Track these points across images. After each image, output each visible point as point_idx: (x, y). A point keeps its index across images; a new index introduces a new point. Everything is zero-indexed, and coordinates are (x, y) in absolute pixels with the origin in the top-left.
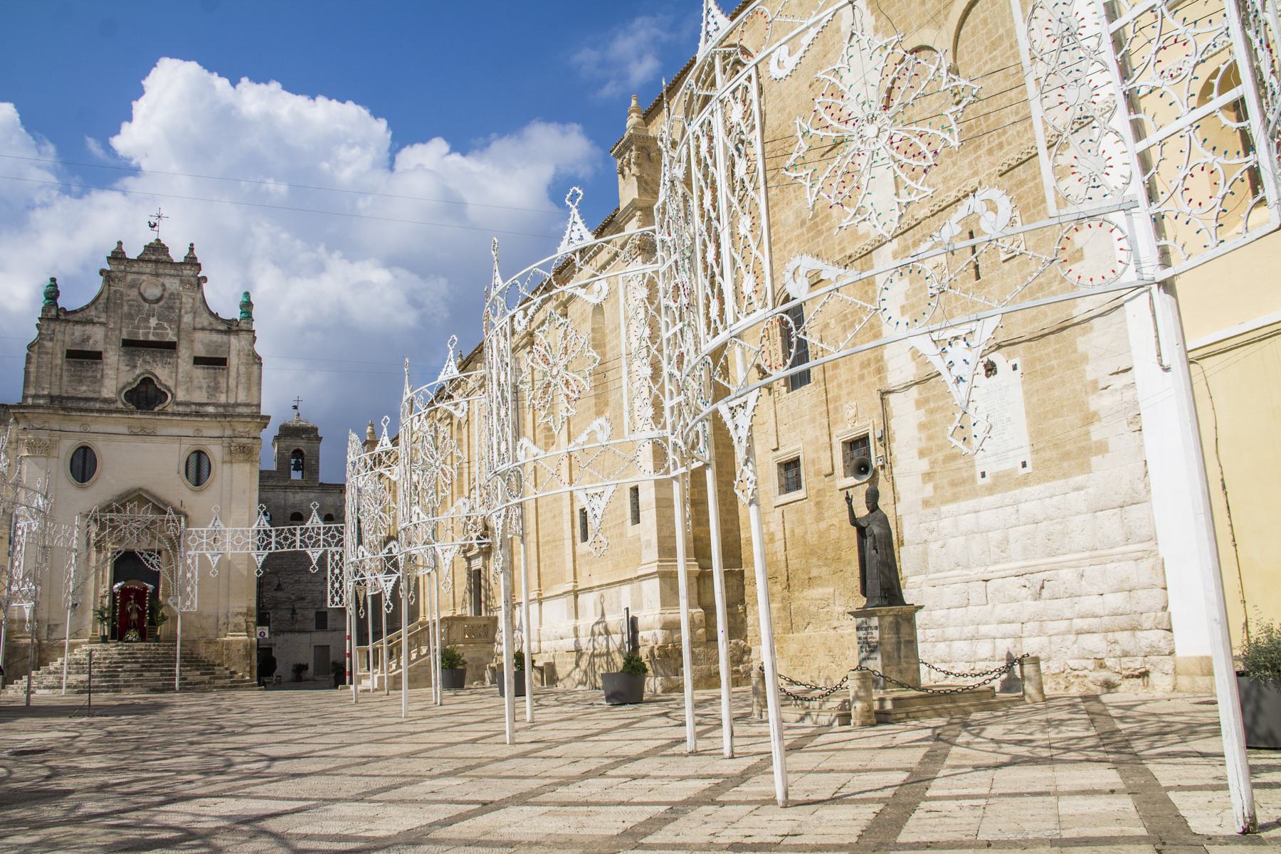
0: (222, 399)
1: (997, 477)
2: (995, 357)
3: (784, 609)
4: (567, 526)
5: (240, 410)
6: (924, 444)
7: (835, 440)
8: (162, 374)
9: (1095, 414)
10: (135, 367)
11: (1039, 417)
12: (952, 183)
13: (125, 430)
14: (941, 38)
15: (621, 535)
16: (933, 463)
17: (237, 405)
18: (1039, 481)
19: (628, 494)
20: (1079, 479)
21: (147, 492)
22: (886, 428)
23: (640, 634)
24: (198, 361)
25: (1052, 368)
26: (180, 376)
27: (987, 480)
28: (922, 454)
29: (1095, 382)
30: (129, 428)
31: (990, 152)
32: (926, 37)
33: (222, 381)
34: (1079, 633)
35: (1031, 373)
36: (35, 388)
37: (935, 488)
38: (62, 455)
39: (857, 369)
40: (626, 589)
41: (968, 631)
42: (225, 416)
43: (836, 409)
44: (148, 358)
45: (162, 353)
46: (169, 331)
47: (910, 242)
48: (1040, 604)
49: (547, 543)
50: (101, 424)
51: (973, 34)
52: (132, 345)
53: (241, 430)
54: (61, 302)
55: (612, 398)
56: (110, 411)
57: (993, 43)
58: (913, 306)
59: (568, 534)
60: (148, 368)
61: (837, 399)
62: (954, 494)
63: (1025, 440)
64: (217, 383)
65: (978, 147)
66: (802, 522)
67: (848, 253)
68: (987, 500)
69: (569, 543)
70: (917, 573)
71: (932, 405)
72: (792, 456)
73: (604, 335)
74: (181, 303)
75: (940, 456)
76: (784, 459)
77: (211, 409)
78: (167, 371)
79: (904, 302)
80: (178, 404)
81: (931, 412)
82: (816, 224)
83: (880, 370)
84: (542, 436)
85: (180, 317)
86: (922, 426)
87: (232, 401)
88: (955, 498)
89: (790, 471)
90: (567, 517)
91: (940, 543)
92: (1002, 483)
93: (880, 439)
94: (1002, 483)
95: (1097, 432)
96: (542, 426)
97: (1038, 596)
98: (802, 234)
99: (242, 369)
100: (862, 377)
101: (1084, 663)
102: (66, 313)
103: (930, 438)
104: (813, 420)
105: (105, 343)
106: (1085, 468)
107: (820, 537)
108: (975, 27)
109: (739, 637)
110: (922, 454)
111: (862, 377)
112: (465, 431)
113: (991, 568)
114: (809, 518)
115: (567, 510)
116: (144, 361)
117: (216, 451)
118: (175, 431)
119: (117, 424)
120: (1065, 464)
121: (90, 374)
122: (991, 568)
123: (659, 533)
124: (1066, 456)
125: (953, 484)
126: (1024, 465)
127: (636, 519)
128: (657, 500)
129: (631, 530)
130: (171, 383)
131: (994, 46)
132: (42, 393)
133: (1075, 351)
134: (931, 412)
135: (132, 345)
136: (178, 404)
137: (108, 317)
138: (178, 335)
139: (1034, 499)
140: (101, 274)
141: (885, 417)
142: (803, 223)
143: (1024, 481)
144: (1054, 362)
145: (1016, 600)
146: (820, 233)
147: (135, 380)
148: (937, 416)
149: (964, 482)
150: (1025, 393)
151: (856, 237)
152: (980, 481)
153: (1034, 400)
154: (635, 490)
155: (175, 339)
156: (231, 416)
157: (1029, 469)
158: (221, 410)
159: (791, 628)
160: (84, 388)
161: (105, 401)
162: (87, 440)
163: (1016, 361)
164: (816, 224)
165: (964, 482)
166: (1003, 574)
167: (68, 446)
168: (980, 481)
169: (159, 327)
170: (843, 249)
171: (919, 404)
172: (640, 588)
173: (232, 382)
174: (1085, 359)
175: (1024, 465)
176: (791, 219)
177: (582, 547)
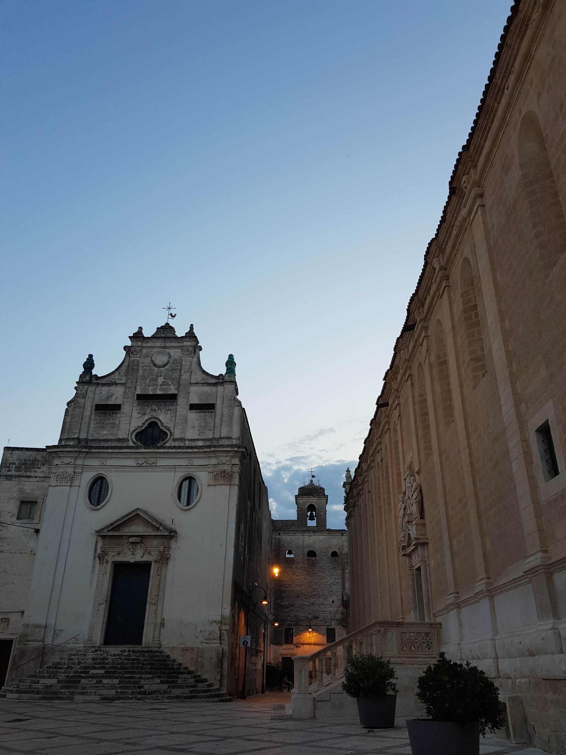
0: (210, 435)
10: (144, 414)
17: (220, 438)
33: (210, 421)
44: (154, 407)
60: (154, 414)
77: (200, 443)
87: (217, 436)
121: (111, 421)
130: (170, 425)
138: (178, 389)
155: (176, 392)
160: (105, 432)
169: (164, 384)
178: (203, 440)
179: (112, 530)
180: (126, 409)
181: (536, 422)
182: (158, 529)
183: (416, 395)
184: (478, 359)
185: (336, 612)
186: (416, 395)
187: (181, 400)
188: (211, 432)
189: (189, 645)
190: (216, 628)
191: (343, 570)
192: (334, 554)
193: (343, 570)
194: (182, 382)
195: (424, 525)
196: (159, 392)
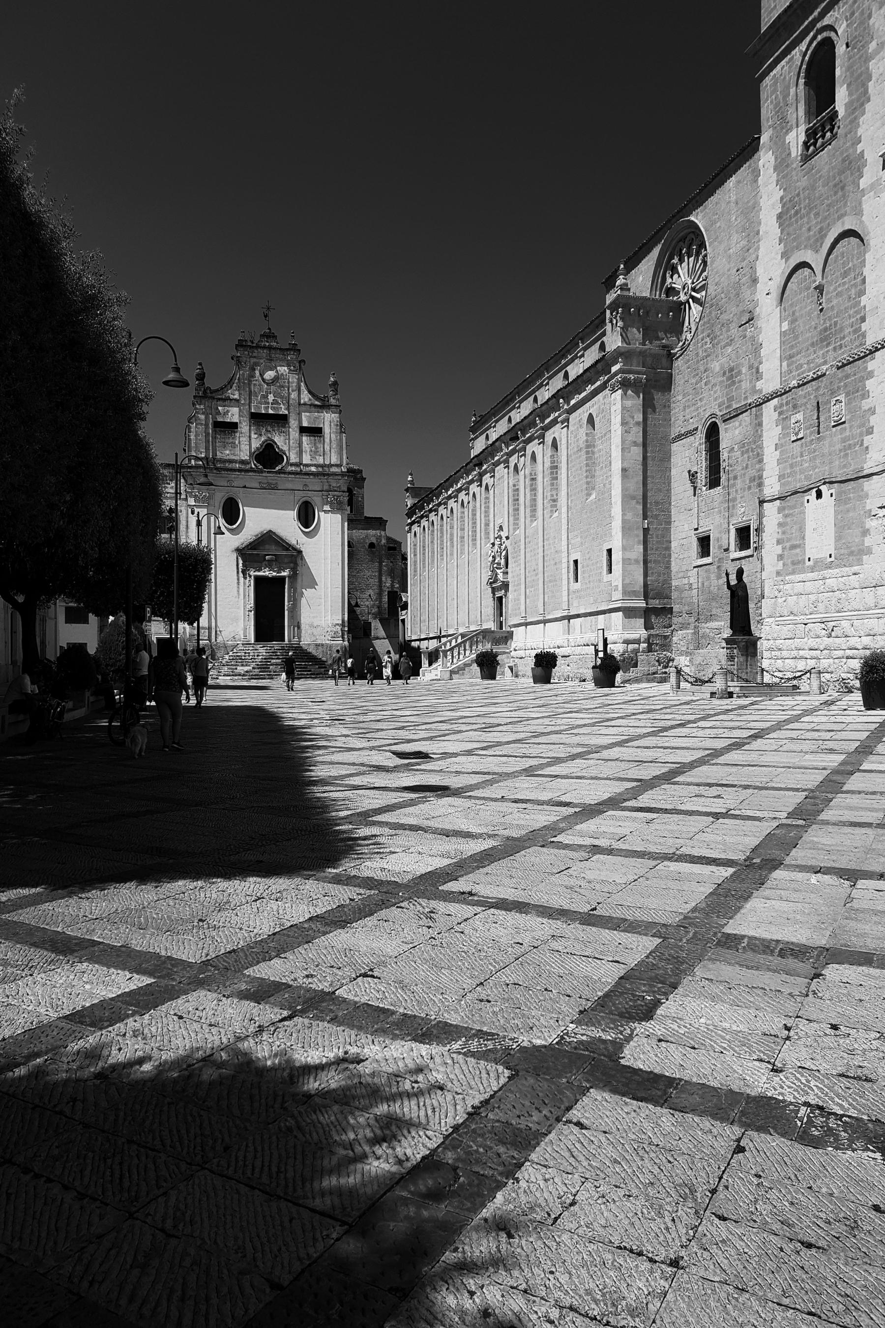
0: (321, 460)
1: (816, 562)
2: (824, 488)
3: (694, 633)
4: (565, 571)
5: (334, 469)
6: (780, 536)
7: (731, 527)
8: (279, 440)
9: (868, 530)
10: (261, 435)
11: (841, 528)
12: (812, 365)
13: (257, 485)
14: (816, 260)
15: (600, 581)
16: (784, 549)
17: (331, 465)
18: (838, 566)
19: (605, 553)
20: (856, 569)
21: (274, 533)
22: (761, 523)
23: (609, 646)
24: (303, 430)
25: (850, 499)
26: (291, 442)
27: (811, 563)
28: (779, 542)
29: (870, 511)
30: (260, 483)
31: (835, 349)
32: (808, 256)
33: (320, 446)
34: (848, 658)
35: (840, 500)
36: (195, 451)
37: (784, 565)
38: (217, 504)
39: (748, 482)
40: (601, 617)
41: (794, 653)
42: (324, 475)
43: (733, 506)
44: (269, 428)
45: (278, 423)
46: (282, 406)
47: (784, 402)
48: (831, 639)
49: (550, 581)
50: (239, 480)
51: (835, 262)
52: (258, 419)
53: (334, 485)
54: (208, 383)
55: (599, 481)
56: (247, 471)
57: (845, 272)
58: (782, 445)
59: (565, 577)
60: (270, 436)
61: (735, 499)
62: (793, 570)
63: (832, 541)
64: (316, 448)
65: (828, 344)
66: (708, 578)
67: (749, 401)
68: (811, 575)
69: (565, 582)
70: (770, 617)
71: (787, 512)
72: (706, 534)
73: (594, 440)
74: (289, 382)
75: (788, 545)
76: (701, 535)
77: (313, 469)
78: (282, 438)
79: (777, 442)
80: (292, 465)
81: (786, 516)
82: (732, 376)
83: (760, 485)
84: (549, 505)
85: (289, 394)
86: (780, 525)
87: (327, 462)
88: (793, 573)
89: (704, 543)
90: (565, 565)
91: (784, 599)
92: (819, 565)
93: (756, 530)
94: (819, 565)
95: (868, 541)
96: (549, 498)
97: (830, 636)
98: (723, 381)
99: (333, 436)
100: (749, 488)
101: (849, 675)
102: (212, 392)
103: (784, 533)
104: (720, 512)
105: (240, 416)
106: (860, 562)
107: (718, 589)
108: (837, 256)
109: (668, 651)
110: (779, 542)
111: (749, 488)
112: (491, 492)
113: (809, 617)
114: (713, 576)
115: (565, 560)
116: (266, 430)
117: (316, 500)
118: (290, 486)
119: (252, 480)
120: (851, 558)
121: (231, 440)
122: (809, 617)
123: (623, 580)
124: (852, 553)
125: (793, 563)
126: (830, 556)
127: (610, 571)
128: (623, 560)
129: (606, 577)
130: (285, 448)
131: (845, 274)
132: (200, 456)
133: (862, 490)
134: (786, 516)
135: (258, 419)
136: (292, 465)
137: (240, 394)
138: (288, 409)
139: (834, 577)
140: (232, 358)
141: (761, 516)
142: (724, 373)
143: (830, 566)
144: (852, 495)
145: (818, 637)
146: (734, 383)
147: (261, 445)
148: (788, 519)
149: (799, 562)
150: (835, 511)
151: (754, 391)
152: (808, 563)
153: (839, 517)
154: (609, 551)
155: (286, 412)
156: (328, 475)
157: (832, 559)
158: (320, 469)
159: (698, 648)
160: (228, 452)
161: (243, 462)
162: (231, 495)
163: (833, 491)
164: (732, 376)
165: (799, 562)
166: (814, 621)
167: (220, 497)
168: (808, 563)
169: (275, 402)
170: (746, 398)
171: (780, 510)
172: (610, 618)
173: (327, 447)
174: (867, 496)
175: (830, 556)
176: (717, 369)
177: (575, 586)
178: (315, 465)
179: (251, 549)
180: (244, 427)
181: (573, 557)
182: (287, 549)
183: (511, 484)
184: (554, 501)
185: (373, 606)
186: (511, 484)
187: (293, 423)
188: (322, 458)
189: (319, 642)
190: (339, 628)
191: (380, 563)
192: (372, 545)
193: (380, 563)
194: (291, 402)
195: (507, 573)
196: (271, 412)
